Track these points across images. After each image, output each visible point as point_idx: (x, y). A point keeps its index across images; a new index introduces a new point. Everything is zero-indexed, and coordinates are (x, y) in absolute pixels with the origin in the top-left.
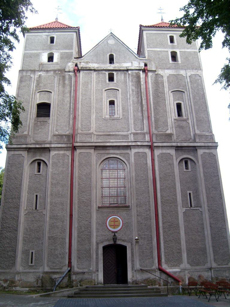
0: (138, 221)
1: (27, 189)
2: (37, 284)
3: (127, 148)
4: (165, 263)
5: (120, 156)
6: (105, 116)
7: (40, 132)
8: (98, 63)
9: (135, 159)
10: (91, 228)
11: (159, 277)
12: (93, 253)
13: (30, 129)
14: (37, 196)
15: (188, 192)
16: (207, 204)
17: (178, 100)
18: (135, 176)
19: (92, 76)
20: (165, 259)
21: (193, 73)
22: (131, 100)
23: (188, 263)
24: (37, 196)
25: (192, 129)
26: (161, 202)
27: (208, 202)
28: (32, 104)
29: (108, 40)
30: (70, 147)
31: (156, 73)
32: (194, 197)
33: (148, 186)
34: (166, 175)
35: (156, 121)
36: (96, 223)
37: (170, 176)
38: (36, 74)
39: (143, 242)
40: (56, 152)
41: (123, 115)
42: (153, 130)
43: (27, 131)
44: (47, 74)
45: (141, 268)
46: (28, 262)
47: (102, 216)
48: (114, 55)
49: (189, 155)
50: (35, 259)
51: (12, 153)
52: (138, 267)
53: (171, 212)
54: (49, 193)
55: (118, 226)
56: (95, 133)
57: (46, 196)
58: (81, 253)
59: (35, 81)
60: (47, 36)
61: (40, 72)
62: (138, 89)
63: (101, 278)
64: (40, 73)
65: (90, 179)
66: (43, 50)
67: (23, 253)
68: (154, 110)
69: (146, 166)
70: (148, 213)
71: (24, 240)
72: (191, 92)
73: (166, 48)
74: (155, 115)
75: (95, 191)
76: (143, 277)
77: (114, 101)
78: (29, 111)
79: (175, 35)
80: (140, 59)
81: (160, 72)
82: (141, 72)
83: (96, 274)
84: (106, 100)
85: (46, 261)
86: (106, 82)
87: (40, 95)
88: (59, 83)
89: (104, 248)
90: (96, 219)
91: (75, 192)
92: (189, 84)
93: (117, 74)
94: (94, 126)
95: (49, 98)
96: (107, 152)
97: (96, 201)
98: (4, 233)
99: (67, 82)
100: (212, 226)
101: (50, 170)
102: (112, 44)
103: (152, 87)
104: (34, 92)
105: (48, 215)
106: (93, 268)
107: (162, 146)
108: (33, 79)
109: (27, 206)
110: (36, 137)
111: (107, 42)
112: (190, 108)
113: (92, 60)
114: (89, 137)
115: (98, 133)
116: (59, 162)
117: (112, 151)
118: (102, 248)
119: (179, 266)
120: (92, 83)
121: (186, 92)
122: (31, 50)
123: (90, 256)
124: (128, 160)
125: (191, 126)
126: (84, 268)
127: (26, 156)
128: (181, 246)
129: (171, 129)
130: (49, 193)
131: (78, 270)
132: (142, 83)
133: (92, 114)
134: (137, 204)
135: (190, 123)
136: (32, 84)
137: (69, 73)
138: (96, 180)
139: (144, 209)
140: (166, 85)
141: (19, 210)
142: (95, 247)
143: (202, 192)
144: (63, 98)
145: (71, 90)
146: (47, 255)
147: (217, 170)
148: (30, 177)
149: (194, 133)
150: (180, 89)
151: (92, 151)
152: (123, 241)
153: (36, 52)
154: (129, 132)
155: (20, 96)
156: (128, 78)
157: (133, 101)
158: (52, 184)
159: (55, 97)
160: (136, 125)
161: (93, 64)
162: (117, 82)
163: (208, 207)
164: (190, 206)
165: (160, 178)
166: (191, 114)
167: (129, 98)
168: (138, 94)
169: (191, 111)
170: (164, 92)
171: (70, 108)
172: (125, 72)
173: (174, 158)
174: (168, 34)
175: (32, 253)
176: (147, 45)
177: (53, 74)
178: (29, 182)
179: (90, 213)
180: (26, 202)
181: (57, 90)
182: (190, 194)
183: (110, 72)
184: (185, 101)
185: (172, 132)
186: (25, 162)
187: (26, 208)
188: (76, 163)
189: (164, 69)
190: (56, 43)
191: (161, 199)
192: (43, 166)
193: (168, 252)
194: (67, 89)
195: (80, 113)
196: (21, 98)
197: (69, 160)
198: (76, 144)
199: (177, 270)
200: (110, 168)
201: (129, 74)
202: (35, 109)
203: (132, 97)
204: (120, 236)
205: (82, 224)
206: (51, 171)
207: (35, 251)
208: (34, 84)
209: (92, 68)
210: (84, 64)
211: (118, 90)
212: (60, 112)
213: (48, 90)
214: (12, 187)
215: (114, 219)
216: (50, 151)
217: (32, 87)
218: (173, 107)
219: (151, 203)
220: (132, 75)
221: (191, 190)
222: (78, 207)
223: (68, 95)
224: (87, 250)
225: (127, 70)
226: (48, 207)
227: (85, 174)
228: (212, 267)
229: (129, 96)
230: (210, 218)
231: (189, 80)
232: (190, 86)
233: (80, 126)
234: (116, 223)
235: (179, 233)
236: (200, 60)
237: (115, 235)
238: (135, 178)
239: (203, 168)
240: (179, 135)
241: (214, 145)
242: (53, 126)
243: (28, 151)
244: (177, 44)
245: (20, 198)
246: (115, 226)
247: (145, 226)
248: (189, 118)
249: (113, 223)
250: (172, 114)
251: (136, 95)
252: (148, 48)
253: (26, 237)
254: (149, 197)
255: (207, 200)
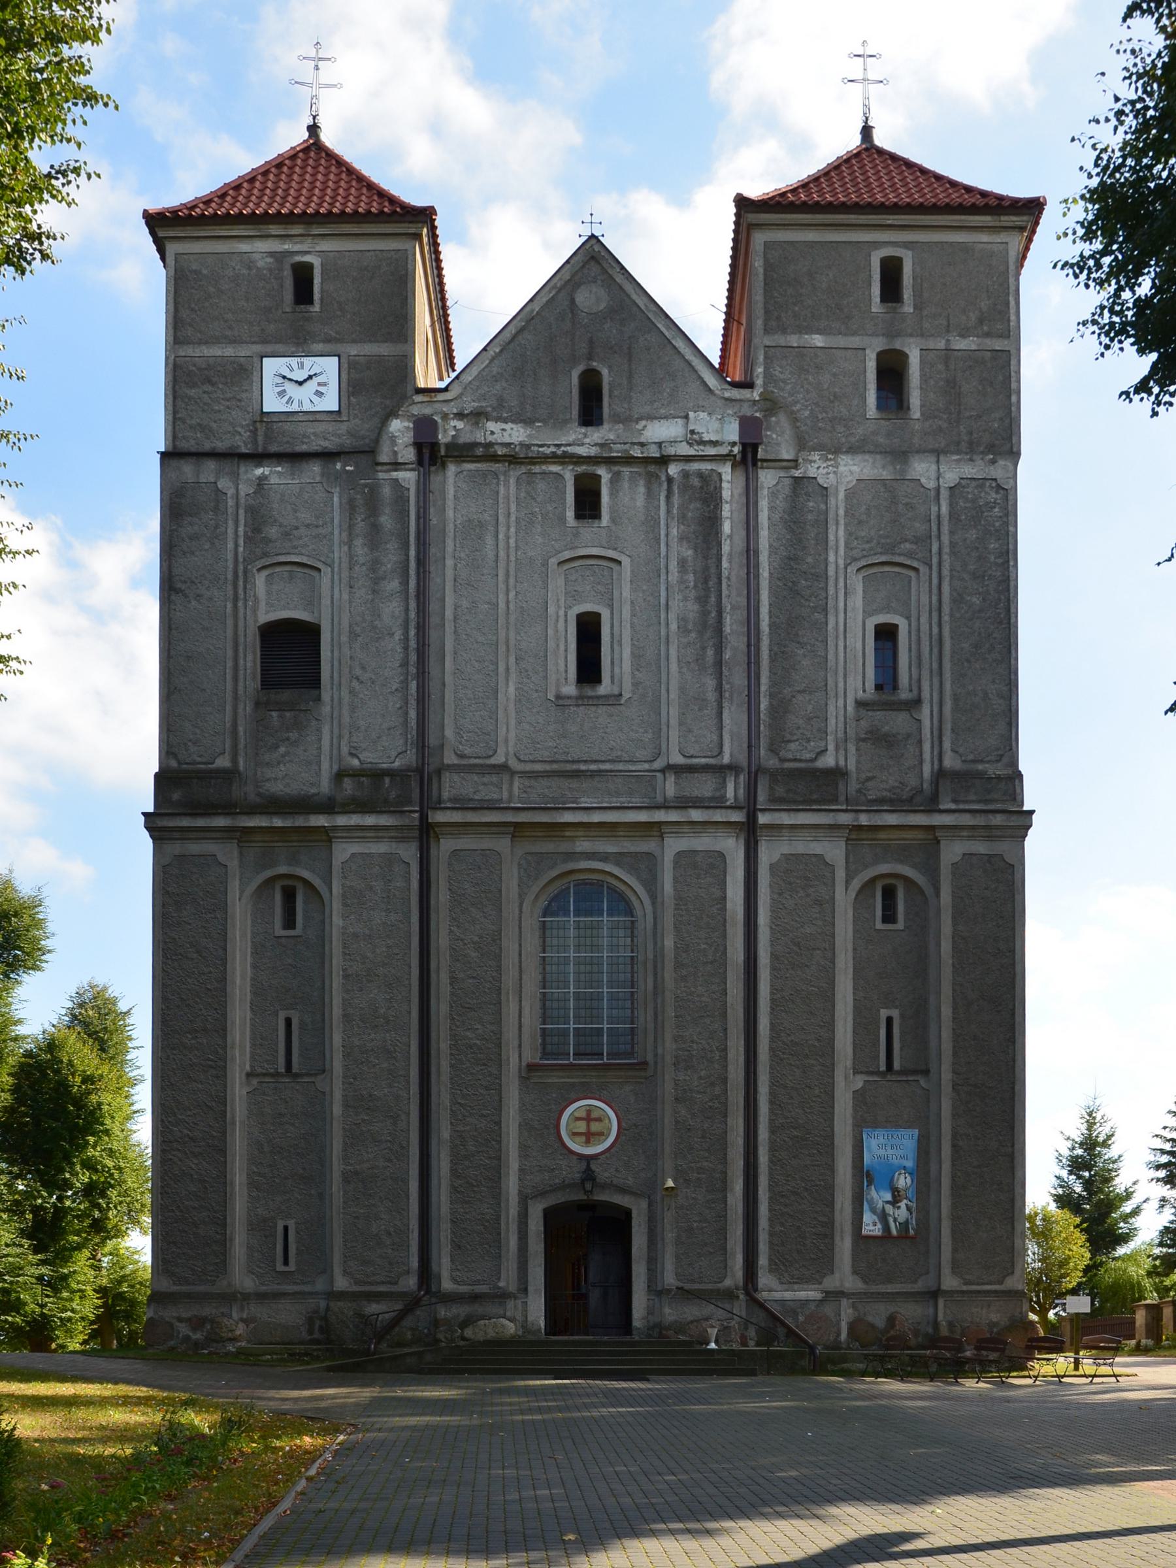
0: (677, 1122)
1: (249, 994)
2: (311, 1332)
3: (648, 833)
4: (770, 1271)
5: (618, 864)
6: (558, 686)
7: (283, 756)
8: (528, 422)
9: (675, 880)
10: (499, 1142)
11: (744, 1316)
12: (508, 1231)
13: (241, 746)
14: (288, 1022)
15: (884, 1013)
16: (954, 1064)
17: (887, 609)
18: (676, 948)
19: (502, 490)
20: (770, 1256)
21: (969, 471)
22: (672, 616)
23: (855, 1272)
24: (288, 1022)
25: (932, 747)
26: (771, 1049)
27: (955, 1054)
28: (236, 626)
29: (577, 285)
30: (409, 828)
31: (797, 473)
32: (902, 1033)
33: (725, 990)
34: (798, 945)
35: (780, 709)
36: (520, 1125)
37: (813, 949)
38: (243, 477)
39: (693, 1195)
40: (355, 848)
41: (636, 685)
42: (762, 752)
43: (226, 754)
44: (293, 474)
45: (681, 1285)
46: (274, 1261)
47: (542, 1101)
48: (605, 372)
49: (902, 862)
50: (297, 1249)
51: (175, 848)
52: (672, 1281)
53: (808, 1090)
54: (337, 1011)
55: (602, 1135)
56: (513, 764)
57: (323, 1020)
58: (465, 1229)
59: (241, 512)
60: (279, 257)
61: (259, 465)
62: (706, 558)
63: (536, 1311)
64: (259, 471)
65: (498, 958)
66: (264, 341)
67: (252, 1229)
68: (773, 660)
69: (718, 909)
70: (717, 1090)
71: (252, 1184)
72: (946, 572)
73: (854, 334)
74: (773, 684)
75: (513, 1007)
76: (685, 1313)
77: (598, 615)
78: (230, 664)
79: (910, 253)
80: (726, 399)
81: (817, 468)
82: (726, 470)
83: (519, 1302)
84: (562, 613)
85: (337, 1258)
86: (562, 519)
87: (269, 580)
88: (351, 527)
89: (549, 1215)
90: (521, 1111)
91: (441, 1008)
92: (945, 528)
93: (616, 479)
94: (512, 735)
95: (312, 601)
96: (565, 847)
97: (520, 1046)
98: (176, 1159)
99: (386, 520)
100: (961, 1143)
101: (337, 920)
102: (594, 311)
103: (770, 546)
104: (241, 567)
105: (338, 1095)
106: (508, 1280)
107: (793, 827)
108: (231, 503)
109: (253, 1058)
110: (268, 780)
111: (573, 301)
112: (935, 651)
113: (501, 401)
114: (492, 784)
115: (528, 767)
116: (371, 888)
117: (583, 845)
118: (541, 1215)
119: (820, 1283)
120: (502, 530)
121: (923, 569)
122: (206, 343)
123: (498, 1243)
124: (652, 884)
125: (929, 736)
126: (477, 1282)
127: (236, 862)
128: (833, 1211)
129: (837, 749)
130: (337, 1011)
131: (455, 1286)
132: (727, 528)
133: (501, 679)
134: (676, 1057)
135: (926, 723)
136: (230, 531)
137: (395, 474)
138: (520, 962)
139: (700, 1078)
140: (838, 534)
141: (225, 1076)
142: (513, 1211)
143: (939, 1016)
144: (370, 597)
145: (408, 560)
146: (342, 1235)
147: (1014, 929)
148: (258, 950)
149: (936, 767)
150: (900, 555)
151: (503, 844)
152: (622, 1190)
153: (229, 351)
154: (658, 765)
155: (179, 585)
156: (662, 498)
157: (682, 620)
158: (346, 977)
159: (336, 596)
160: (690, 731)
161: (504, 426)
162: (613, 520)
163: (954, 1072)
164: (883, 1068)
165: (774, 957)
166: (936, 681)
167: (663, 601)
168: (706, 581)
169: (935, 666)
170: (826, 570)
171: (406, 648)
172: (652, 468)
173: (840, 874)
174: (876, 245)
175: (286, 1228)
176: (767, 312)
177: (323, 475)
178: (254, 966)
179: (497, 1089)
180: (248, 1045)
181: (345, 560)
182: (889, 1020)
183: (581, 469)
184: (914, 613)
185: (842, 763)
186: (234, 886)
187: (251, 1066)
188: (441, 896)
189: (837, 451)
190: (322, 300)
191: (772, 1040)
192: (305, 902)
193: (781, 1231)
194: (390, 558)
195: (448, 678)
196: (186, 596)
197: (408, 881)
198: (439, 817)
199: (810, 1293)
200: (549, 1047)
201: (670, 480)
202: (254, 653)
203: (678, 597)
204: (606, 1174)
205: (468, 1128)
206: (341, 923)
207: (296, 1223)
208: (237, 526)
209: (500, 451)
210: (460, 425)
211: (619, 563)
212: (363, 668)
213: (305, 560)
214: (189, 990)
215: (589, 1112)
216: (330, 841)
217: (230, 546)
218: (859, 645)
219: (731, 1055)
220: (685, 487)
221: (896, 1007)
222: (452, 1066)
223: (394, 585)
224: (488, 1221)
225: (664, 461)
226: (338, 1065)
227: (476, 939)
228: (944, 1287)
229: (663, 594)
230: (955, 1116)
231: (944, 509)
232: (946, 539)
233: (449, 733)
234: (595, 1127)
235: (831, 1168)
236: (1014, 399)
237: (588, 1168)
238: (675, 958)
239: (954, 918)
240: (870, 774)
241: (1015, 821)
242: (336, 731)
243: (239, 841)
244: (915, 307)
245: (225, 1030)
246: (589, 1137)
247: (703, 1137)
248: (926, 694)
249: (581, 1127)
250: (850, 680)
251: (695, 586)
252: (767, 331)
253: (259, 1174)
254: (726, 1030)
255: (954, 1047)
